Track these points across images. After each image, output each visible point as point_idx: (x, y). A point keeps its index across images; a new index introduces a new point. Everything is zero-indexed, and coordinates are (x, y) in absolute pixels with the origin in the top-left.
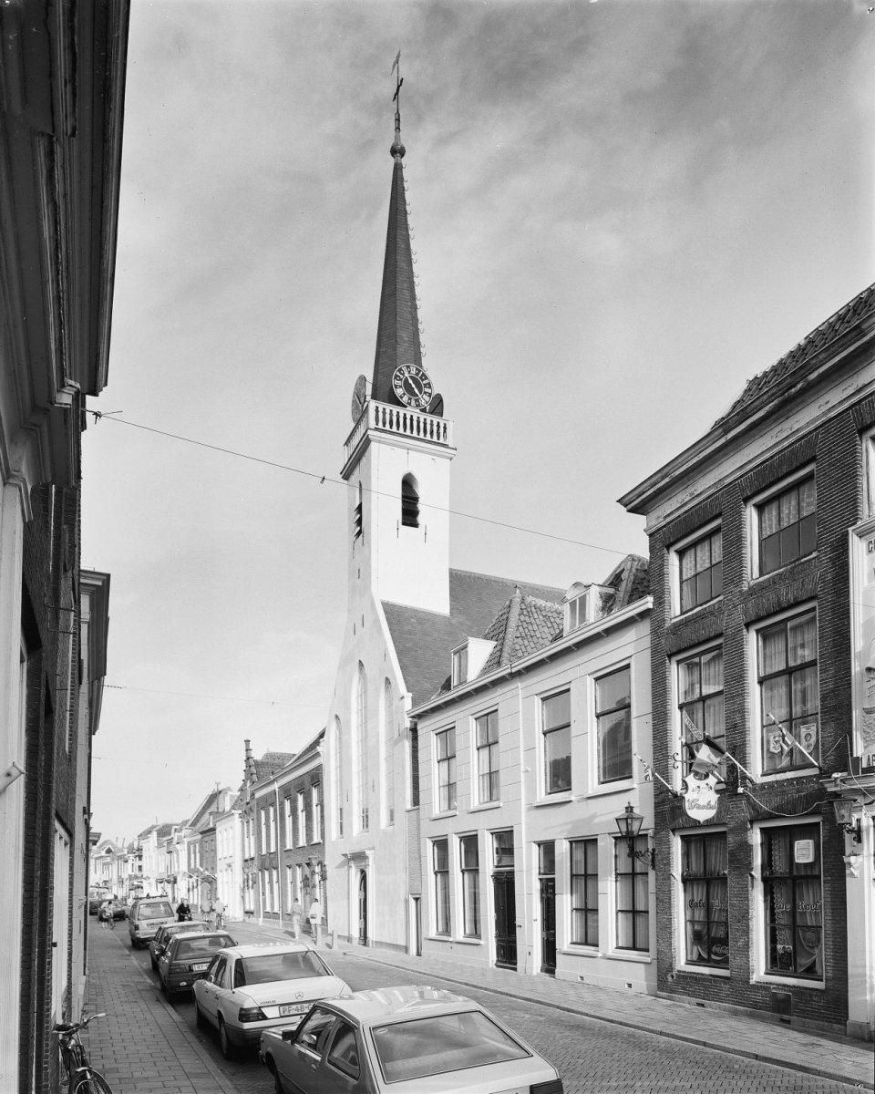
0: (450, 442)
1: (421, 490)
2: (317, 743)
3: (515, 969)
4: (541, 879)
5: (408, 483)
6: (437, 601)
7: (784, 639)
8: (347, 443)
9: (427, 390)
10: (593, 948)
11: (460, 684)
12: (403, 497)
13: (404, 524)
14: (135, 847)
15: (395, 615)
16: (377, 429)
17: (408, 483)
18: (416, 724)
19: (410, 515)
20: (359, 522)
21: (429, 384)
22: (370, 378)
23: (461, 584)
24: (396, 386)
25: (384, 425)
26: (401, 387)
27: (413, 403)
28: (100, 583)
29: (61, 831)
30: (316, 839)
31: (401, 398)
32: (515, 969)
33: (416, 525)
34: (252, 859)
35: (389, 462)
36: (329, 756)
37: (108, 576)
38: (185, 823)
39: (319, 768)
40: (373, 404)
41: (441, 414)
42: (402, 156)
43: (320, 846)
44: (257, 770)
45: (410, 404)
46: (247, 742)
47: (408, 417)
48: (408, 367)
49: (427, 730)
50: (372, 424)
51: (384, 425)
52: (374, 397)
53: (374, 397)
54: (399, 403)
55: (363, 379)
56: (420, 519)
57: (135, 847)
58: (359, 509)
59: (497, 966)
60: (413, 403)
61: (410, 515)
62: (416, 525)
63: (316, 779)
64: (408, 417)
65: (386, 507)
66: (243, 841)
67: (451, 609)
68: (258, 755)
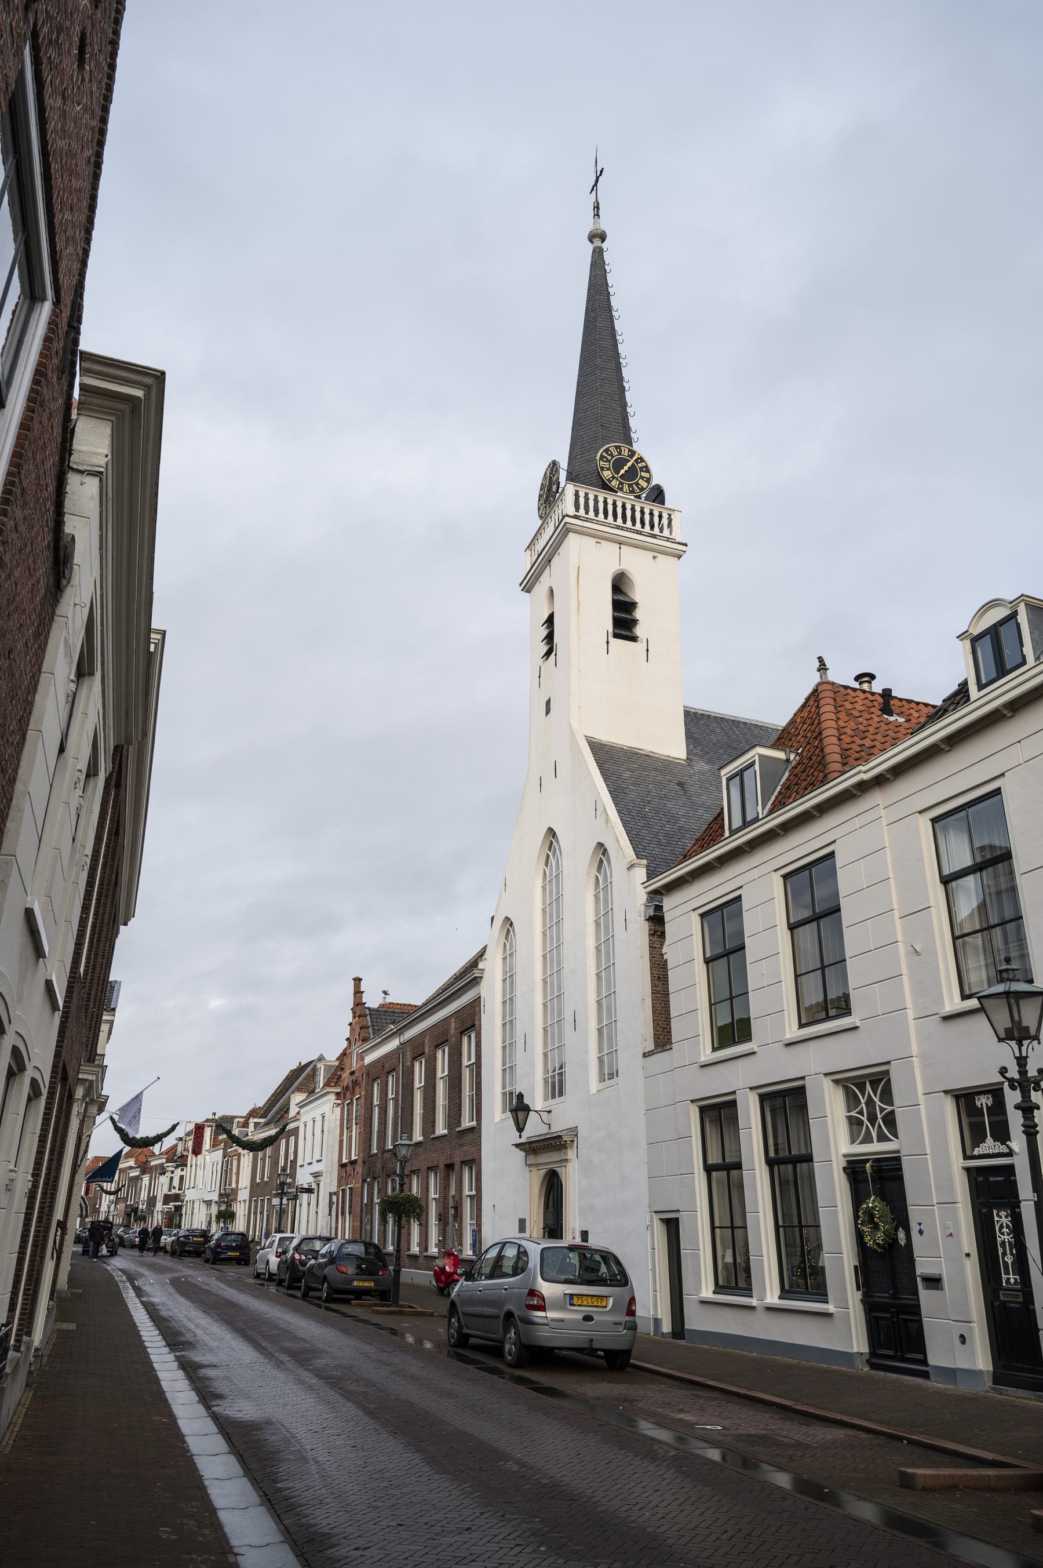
1: (638, 594)
2: (474, 964)
4: (968, 1170)
6: (672, 745)
7: (58, 1286)
9: (643, 474)
11: (745, 824)
13: (616, 636)
14: (178, 1154)
15: (609, 758)
16: (576, 517)
17: (619, 584)
18: (659, 908)
19: (624, 621)
20: (550, 638)
21: (647, 467)
22: (564, 464)
23: (697, 724)
24: (602, 469)
26: (609, 469)
27: (626, 488)
28: (139, 393)
29: (332, 1550)
30: (466, 1123)
34: (353, 1163)
35: (588, 566)
36: (491, 991)
37: (160, 377)
38: (253, 1113)
39: (477, 1002)
40: (570, 489)
42: (603, 241)
43: (475, 1132)
44: (370, 1021)
46: (358, 981)
47: (619, 504)
48: (617, 447)
49: (684, 916)
52: (571, 478)
53: (571, 478)
54: (605, 486)
55: (554, 466)
56: (639, 631)
57: (178, 1154)
58: (550, 621)
59: (873, 1366)
60: (626, 488)
61: (624, 621)
62: (634, 639)
63: (469, 1021)
64: (619, 504)
66: (341, 1134)
68: (372, 1000)
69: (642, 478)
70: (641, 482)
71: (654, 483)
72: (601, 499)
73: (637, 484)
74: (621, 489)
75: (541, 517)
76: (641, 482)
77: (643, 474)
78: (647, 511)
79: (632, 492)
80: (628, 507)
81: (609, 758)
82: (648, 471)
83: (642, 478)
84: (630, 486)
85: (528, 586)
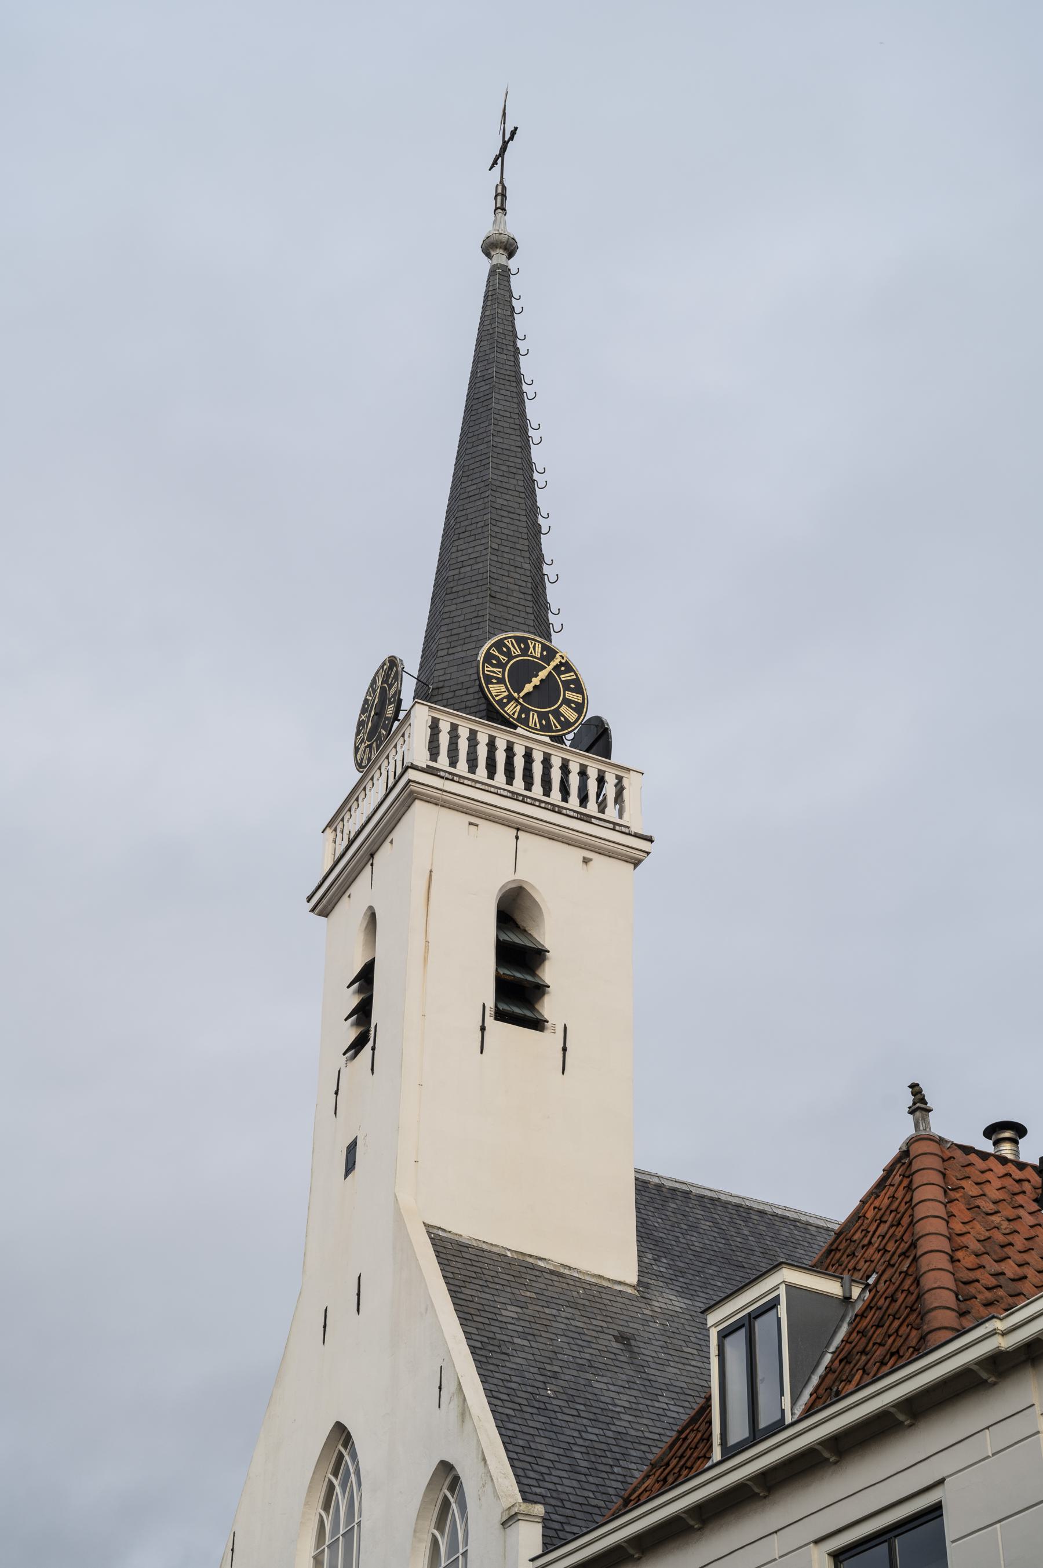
0: (633, 819)
1: (549, 933)
3: (636, 1171)
5: (513, 910)
8: (309, 899)
9: (570, 695)
10: (649, 843)
12: (543, 1535)
13: (501, 1016)
15: (475, 1275)
17: (513, 910)
20: (363, 1013)
22: (412, 664)
23: (662, 1208)
24: (489, 679)
25: (453, 763)
26: (501, 681)
27: (534, 719)
31: (503, 706)
32: (636, 1171)
33: (537, 1024)
35: (449, 870)
40: (421, 716)
41: (607, 754)
45: (525, 722)
50: (422, 758)
51: (453, 763)
52: (424, 693)
53: (424, 693)
54: (493, 714)
55: (392, 668)
56: (548, 1008)
58: (366, 977)
60: (534, 719)
62: (537, 1024)
65: (449, 969)
67: (641, 1273)
69: (567, 702)
70: (564, 709)
71: (590, 713)
72: (483, 739)
73: (557, 714)
74: (525, 722)
75: (359, 766)
76: (564, 709)
77: (570, 695)
78: (574, 768)
79: (546, 728)
80: (538, 757)
81: (475, 1275)
82: (579, 689)
83: (567, 702)
84: (542, 716)
85: (325, 903)
